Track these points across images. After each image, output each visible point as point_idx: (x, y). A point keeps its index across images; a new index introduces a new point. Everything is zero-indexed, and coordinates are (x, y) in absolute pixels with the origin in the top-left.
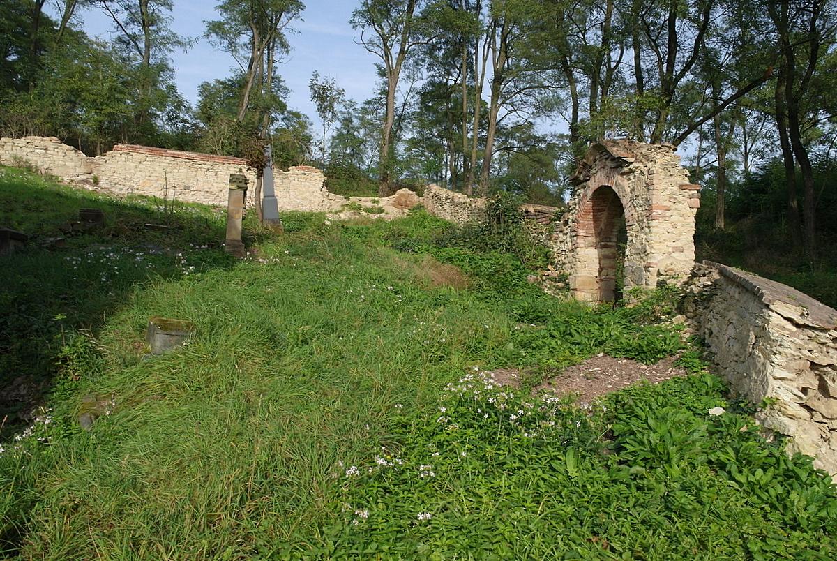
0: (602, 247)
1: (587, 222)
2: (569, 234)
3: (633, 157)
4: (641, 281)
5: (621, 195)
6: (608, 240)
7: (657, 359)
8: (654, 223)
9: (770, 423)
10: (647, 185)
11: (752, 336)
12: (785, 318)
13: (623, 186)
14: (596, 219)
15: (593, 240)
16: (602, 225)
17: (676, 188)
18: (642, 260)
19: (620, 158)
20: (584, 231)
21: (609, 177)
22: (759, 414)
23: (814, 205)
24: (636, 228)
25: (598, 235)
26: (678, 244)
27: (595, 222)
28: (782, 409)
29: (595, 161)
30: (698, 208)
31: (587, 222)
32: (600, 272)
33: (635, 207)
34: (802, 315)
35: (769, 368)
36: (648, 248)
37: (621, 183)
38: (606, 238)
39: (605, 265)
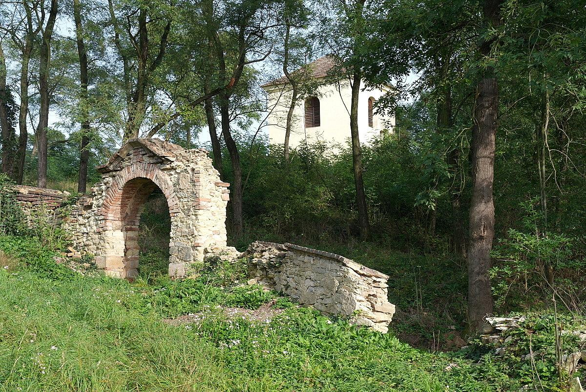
0: (127, 230)
1: (115, 208)
2: (92, 218)
3: (174, 157)
4: (190, 257)
5: (163, 187)
6: (133, 223)
7: (258, 306)
8: (200, 212)
9: (359, 322)
10: (193, 181)
11: (337, 282)
12: (355, 271)
13: (164, 180)
14: (123, 205)
15: (119, 223)
16: (128, 210)
17: (213, 185)
18: (189, 241)
19: (164, 157)
20: (112, 215)
21: (147, 171)
22: (352, 320)
23: (241, 191)
24: (181, 215)
25: (123, 219)
26: (215, 229)
27: (122, 208)
28: (365, 315)
29: (128, 155)
30: (228, 201)
31: (115, 208)
32: (125, 252)
33: (179, 198)
34: (361, 269)
35: (354, 296)
36: (195, 231)
37: (163, 177)
38: (131, 222)
39: (131, 247)
